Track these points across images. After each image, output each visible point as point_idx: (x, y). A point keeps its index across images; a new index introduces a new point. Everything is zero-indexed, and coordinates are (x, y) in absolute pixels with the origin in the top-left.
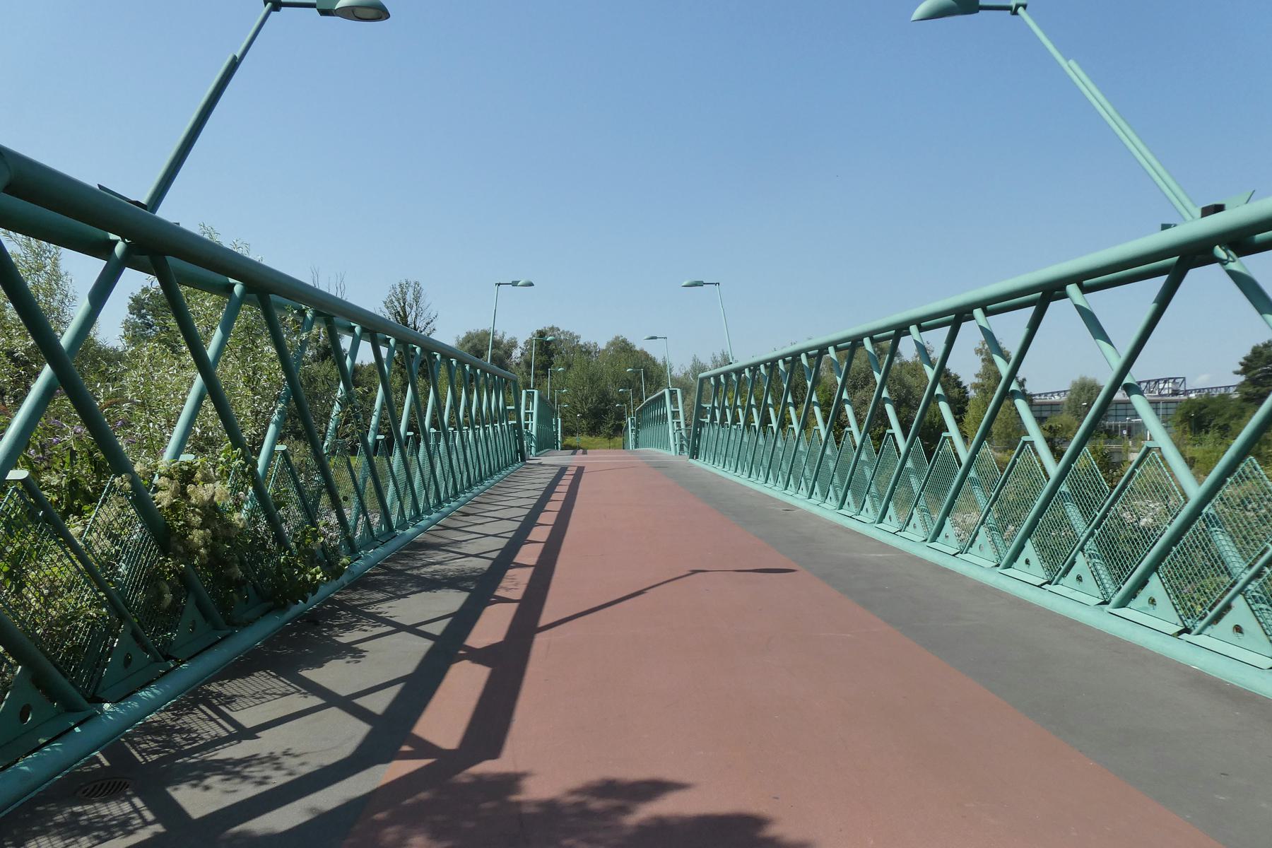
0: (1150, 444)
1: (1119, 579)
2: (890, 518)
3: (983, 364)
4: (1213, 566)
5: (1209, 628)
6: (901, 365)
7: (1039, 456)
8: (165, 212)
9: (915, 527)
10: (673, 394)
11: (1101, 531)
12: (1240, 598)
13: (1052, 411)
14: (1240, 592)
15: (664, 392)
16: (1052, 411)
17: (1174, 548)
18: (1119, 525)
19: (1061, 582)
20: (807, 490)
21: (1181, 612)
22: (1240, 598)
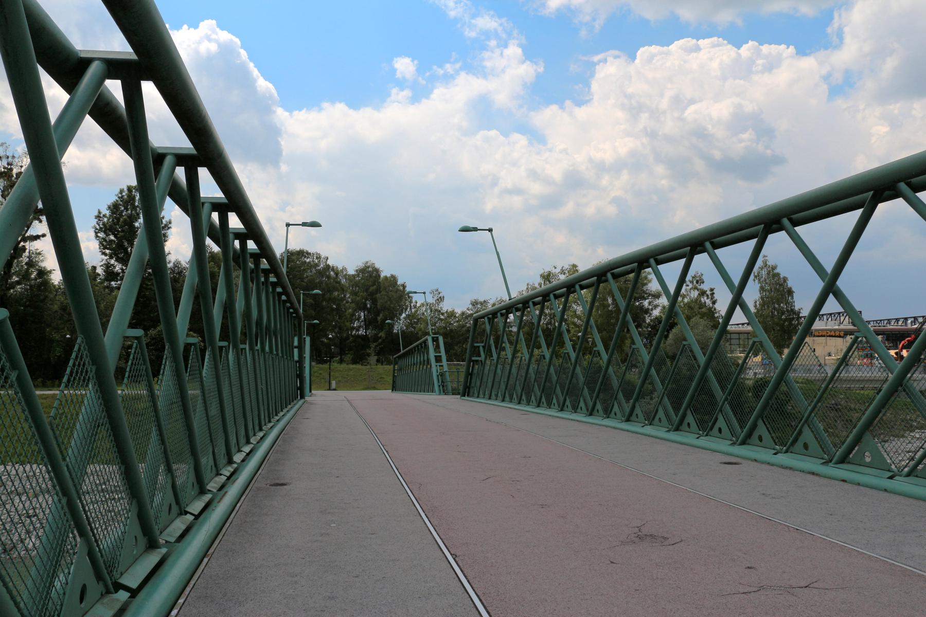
0: (755, 339)
1: (742, 424)
2: (598, 410)
3: (781, 277)
4: (757, 392)
5: (792, 447)
6: (787, 327)
7: (697, 361)
8: (514, 295)
9: (615, 414)
10: (435, 340)
11: (732, 397)
12: (806, 426)
13: (739, 339)
14: (806, 421)
15: (427, 340)
16: (739, 339)
17: (770, 402)
18: (785, 426)
19: (709, 434)
20: (536, 402)
21: (773, 435)
22: (806, 426)
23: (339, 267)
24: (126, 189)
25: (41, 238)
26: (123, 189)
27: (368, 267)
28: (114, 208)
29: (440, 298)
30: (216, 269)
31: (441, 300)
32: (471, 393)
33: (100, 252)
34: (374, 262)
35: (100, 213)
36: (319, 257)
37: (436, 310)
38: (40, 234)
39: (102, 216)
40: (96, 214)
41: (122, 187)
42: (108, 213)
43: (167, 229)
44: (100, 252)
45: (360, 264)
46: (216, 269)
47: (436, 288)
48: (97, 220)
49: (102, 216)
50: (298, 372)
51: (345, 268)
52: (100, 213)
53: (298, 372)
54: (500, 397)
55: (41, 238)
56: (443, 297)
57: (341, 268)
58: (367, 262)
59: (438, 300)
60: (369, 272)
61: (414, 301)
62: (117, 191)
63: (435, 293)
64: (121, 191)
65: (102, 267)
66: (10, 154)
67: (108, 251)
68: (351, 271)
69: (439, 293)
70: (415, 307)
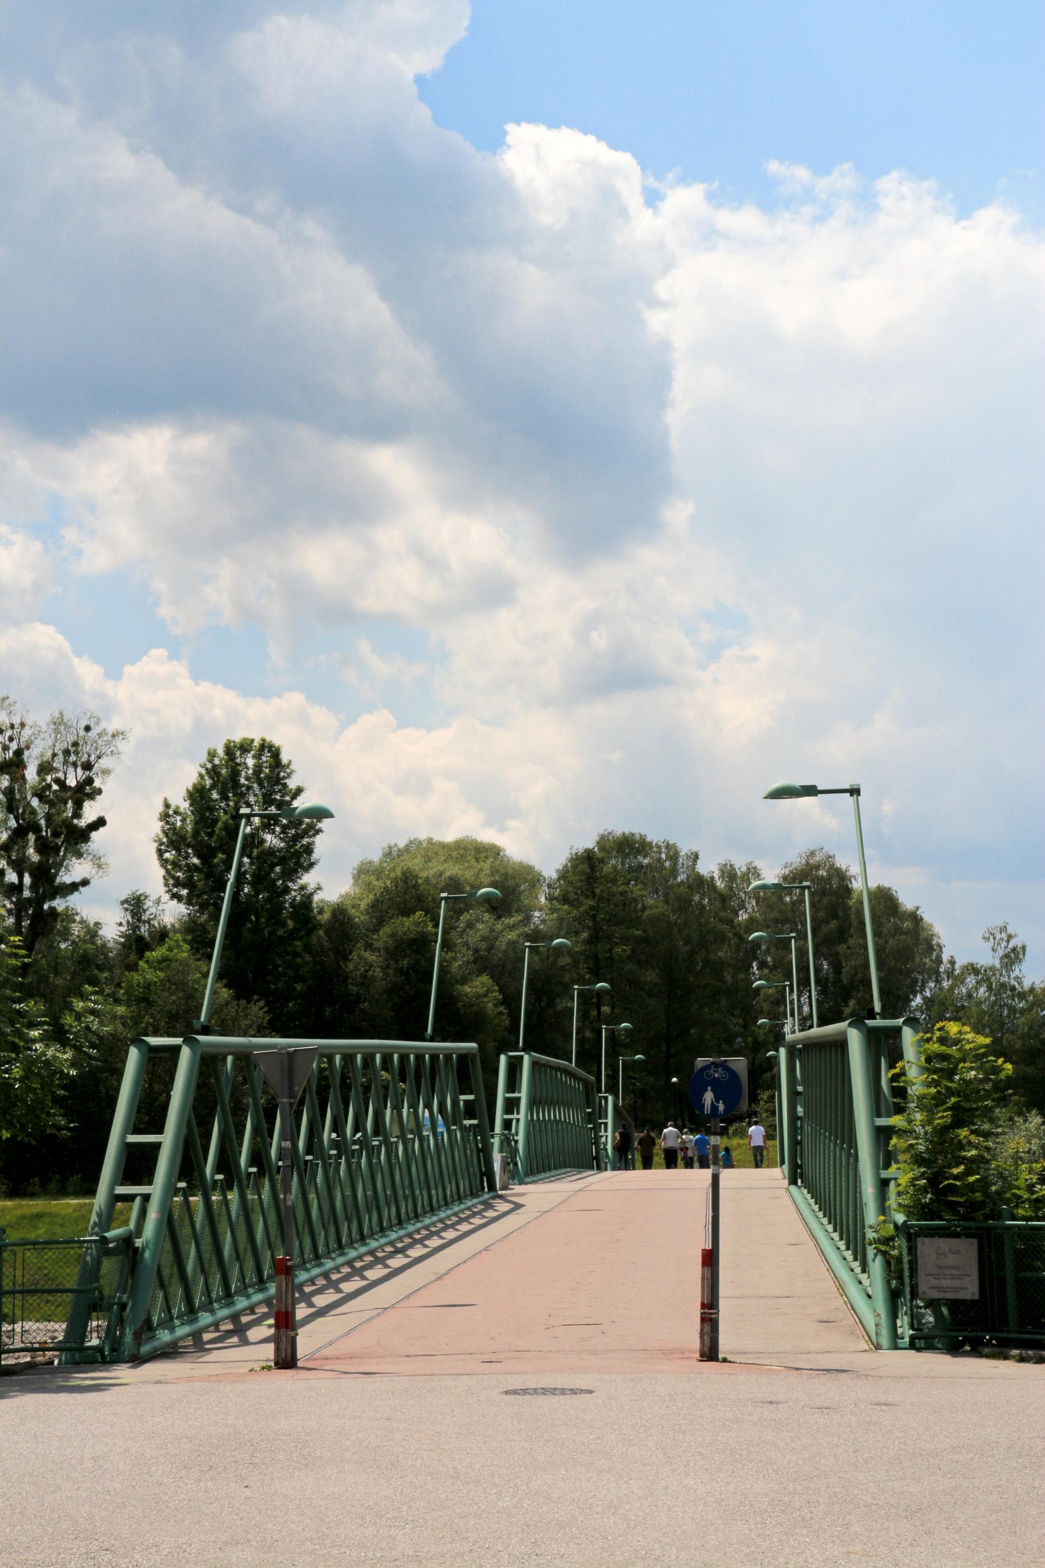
23: (737, 867)
24: (221, 752)
25: (81, 889)
26: (215, 751)
27: (817, 867)
28: (198, 796)
29: (1014, 950)
30: (430, 928)
31: (1017, 957)
32: (603, 1166)
33: (168, 892)
34: (831, 854)
35: (167, 806)
36: (673, 854)
37: (1003, 986)
38: (78, 880)
39: (171, 812)
40: (161, 808)
41: (212, 746)
42: (185, 806)
43: (314, 835)
44: (168, 892)
45: (795, 859)
46: (430, 928)
47: (1000, 924)
48: (163, 823)
49: (171, 812)
50: (480, 1145)
51: (755, 868)
52: (167, 806)
53: (480, 1145)
54: (638, 1164)
55: (81, 889)
56: (1024, 948)
57: (744, 869)
58: (813, 853)
59: (1007, 956)
60: (820, 880)
61: (945, 958)
62: (203, 758)
63: (998, 936)
64: (212, 755)
65: (126, 906)
66: (16, 721)
67: (184, 892)
68: (771, 876)
69: (1010, 937)
70: (950, 974)
